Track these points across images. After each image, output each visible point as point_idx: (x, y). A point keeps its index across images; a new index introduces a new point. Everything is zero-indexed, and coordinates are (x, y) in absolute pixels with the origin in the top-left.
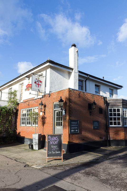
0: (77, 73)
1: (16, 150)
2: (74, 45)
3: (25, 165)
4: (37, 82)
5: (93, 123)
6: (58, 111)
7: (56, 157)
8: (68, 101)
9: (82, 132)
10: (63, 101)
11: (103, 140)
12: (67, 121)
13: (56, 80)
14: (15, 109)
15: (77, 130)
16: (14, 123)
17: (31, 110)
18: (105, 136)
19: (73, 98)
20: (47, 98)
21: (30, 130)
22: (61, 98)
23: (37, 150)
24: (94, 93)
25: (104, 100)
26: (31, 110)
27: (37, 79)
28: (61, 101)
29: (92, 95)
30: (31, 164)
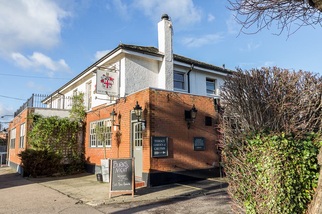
0: (171, 61)
1: (78, 183)
2: (166, 17)
3: (78, 201)
4: (105, 80)
5: (194, 142)
6: (137, 124)
7: (124, 191)
8: (149, 108)
9: (174, 155)
10: (140, 108)
11: (212, 167)
12: (148, 138)
14: (82, 122)
15: (164, 153)
16: (81, 143)
17: (103, 122)
18: (216, 161)
19: (157, 103)
20: (122, 104)
21: (101, 154)
22: (137, 103)
23: (108, 183)
24: (205, 94)
25: (215, 103)
26: (103, 122)
27: (106, 75)
28: (138, 108)
29: (192, 96)
30: (87, 200)
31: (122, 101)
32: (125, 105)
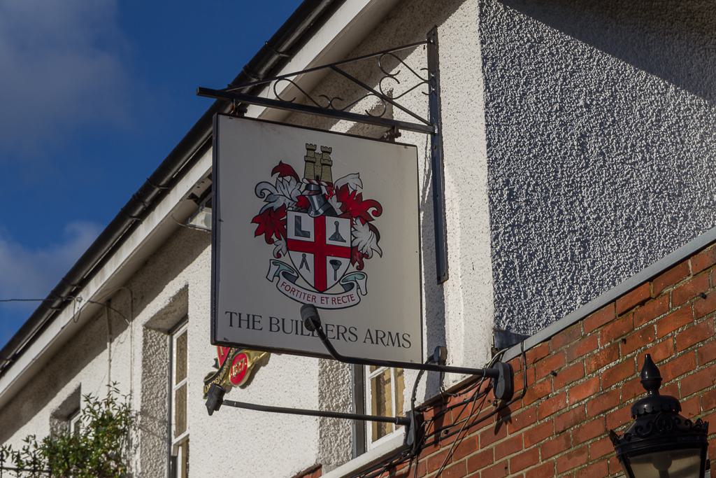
4: (291, 216)
13: (593, 146)
20: (472, 445)
27: (300, 168)
31: (466, 418)
32: (501, 451)
